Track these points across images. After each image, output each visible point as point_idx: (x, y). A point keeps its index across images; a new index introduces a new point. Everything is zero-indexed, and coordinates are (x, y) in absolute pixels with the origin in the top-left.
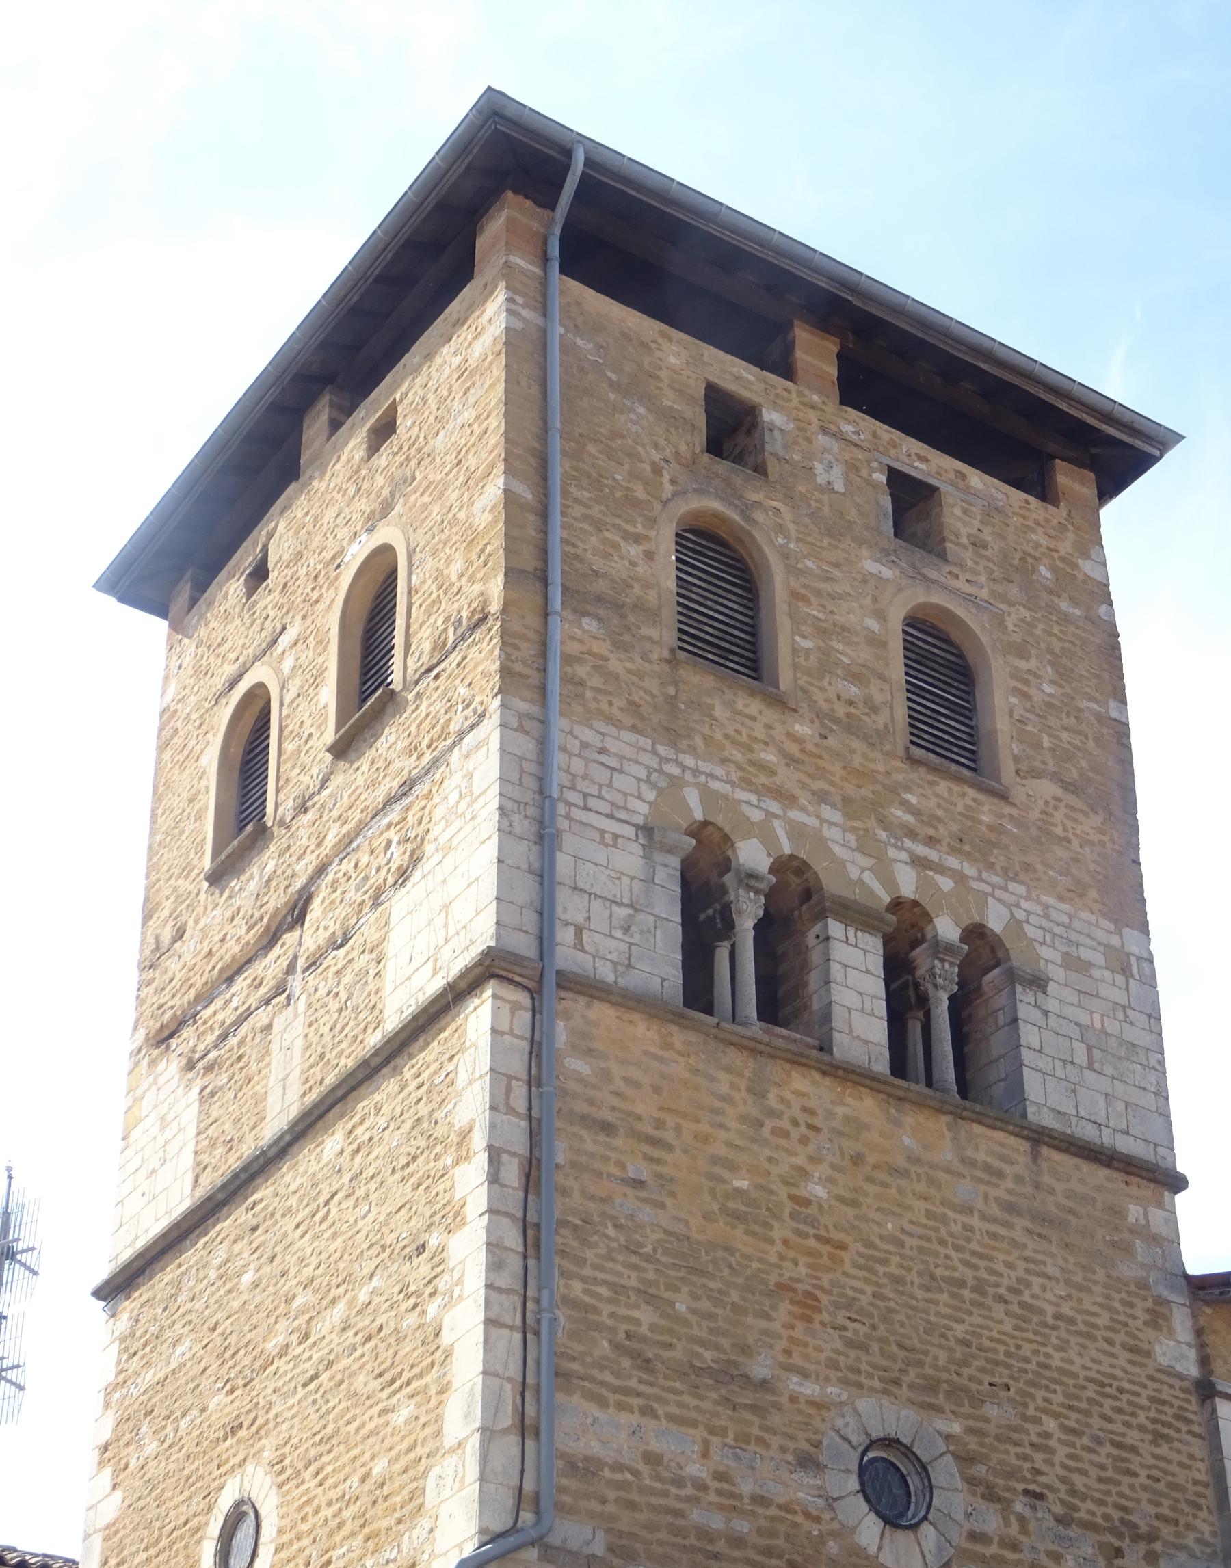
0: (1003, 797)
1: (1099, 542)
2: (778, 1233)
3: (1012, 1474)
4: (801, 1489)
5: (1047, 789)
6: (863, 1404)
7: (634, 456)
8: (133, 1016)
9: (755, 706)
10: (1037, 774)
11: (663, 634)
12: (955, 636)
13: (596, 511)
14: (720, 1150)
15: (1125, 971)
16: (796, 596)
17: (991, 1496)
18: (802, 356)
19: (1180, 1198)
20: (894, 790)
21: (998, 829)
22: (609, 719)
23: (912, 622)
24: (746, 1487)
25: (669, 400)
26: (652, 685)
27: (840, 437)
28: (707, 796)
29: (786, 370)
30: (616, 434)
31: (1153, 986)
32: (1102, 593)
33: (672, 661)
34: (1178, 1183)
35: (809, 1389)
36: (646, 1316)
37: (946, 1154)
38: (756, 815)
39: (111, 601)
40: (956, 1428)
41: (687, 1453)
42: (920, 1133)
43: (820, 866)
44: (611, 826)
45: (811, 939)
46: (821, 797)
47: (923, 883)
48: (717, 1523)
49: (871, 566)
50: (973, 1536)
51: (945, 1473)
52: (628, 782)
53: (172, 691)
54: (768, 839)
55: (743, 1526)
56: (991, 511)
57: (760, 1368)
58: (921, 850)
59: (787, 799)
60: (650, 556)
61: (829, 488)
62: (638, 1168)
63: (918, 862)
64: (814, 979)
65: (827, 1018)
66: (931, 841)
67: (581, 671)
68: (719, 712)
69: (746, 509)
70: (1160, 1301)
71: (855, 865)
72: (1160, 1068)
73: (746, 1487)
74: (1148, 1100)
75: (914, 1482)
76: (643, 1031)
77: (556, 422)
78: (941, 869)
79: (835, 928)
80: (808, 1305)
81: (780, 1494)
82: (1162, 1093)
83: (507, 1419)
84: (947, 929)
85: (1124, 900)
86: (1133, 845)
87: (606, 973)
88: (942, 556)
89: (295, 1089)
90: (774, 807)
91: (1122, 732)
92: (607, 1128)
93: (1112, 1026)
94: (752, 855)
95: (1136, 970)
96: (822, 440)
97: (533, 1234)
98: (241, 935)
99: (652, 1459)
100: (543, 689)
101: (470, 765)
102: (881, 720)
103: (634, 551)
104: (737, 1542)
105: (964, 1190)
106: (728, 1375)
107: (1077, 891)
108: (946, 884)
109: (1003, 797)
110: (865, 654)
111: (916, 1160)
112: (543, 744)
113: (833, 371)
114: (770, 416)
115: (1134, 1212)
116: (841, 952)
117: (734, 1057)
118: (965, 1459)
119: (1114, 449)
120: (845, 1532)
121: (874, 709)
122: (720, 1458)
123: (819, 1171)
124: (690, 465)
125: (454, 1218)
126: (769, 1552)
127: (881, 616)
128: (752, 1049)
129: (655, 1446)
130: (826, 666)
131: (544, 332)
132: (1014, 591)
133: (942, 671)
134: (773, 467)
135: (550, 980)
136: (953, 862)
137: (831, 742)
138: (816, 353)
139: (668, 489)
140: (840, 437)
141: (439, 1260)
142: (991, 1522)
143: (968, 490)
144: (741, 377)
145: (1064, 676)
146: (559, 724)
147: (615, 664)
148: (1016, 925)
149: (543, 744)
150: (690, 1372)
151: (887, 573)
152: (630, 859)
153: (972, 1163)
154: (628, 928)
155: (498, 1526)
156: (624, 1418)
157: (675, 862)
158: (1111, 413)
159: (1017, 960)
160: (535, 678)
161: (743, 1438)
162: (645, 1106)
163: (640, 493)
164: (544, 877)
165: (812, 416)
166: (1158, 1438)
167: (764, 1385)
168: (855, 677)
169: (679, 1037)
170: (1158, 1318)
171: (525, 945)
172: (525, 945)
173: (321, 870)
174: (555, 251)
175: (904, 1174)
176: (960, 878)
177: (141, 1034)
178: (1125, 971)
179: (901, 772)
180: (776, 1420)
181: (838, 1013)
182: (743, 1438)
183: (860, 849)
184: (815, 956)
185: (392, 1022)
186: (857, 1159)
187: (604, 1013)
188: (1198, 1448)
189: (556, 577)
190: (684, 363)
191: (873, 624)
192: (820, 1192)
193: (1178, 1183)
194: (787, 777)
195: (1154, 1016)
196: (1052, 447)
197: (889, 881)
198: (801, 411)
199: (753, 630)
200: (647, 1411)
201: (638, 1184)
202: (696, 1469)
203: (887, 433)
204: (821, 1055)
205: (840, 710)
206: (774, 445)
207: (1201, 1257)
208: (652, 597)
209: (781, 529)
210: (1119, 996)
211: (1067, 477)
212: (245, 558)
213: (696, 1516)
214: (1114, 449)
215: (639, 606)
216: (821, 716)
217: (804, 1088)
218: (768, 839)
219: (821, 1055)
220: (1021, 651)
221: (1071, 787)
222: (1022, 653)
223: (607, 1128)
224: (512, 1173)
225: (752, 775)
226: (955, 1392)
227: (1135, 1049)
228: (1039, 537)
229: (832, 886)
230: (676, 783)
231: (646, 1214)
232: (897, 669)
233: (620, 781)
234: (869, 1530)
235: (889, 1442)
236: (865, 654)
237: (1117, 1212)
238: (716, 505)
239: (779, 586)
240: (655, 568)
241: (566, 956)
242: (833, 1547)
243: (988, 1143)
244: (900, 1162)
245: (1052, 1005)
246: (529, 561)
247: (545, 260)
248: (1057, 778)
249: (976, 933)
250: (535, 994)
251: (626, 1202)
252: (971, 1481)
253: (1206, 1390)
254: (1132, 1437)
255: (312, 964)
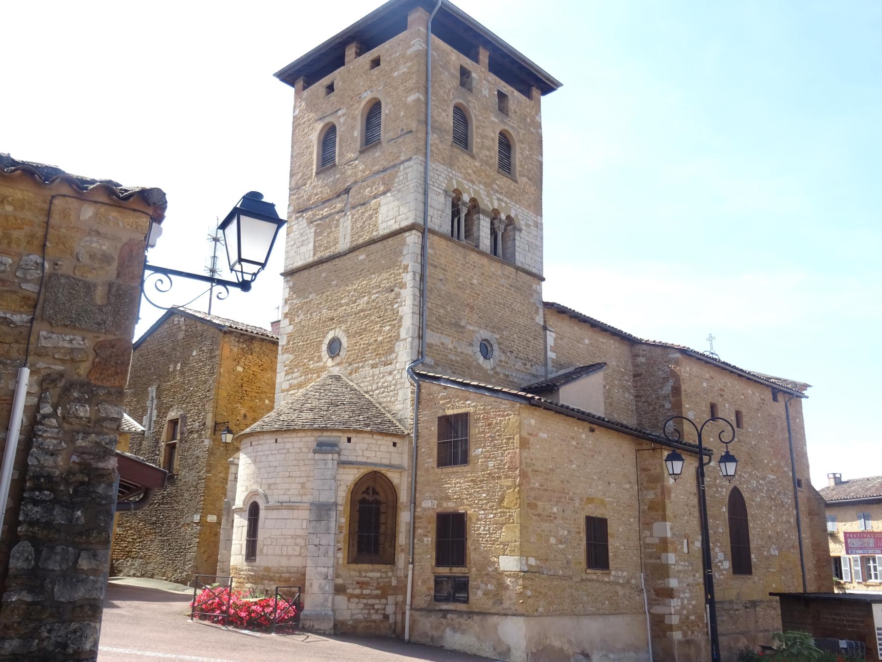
0: (516, 182)
1: (540, 111)
2: (468, 291)
3: (507, 347)
4: (469, 351)
5: (525, 179)
7: (444, 87)
9: (468, 158)
12: (508, 137)
14: (457, 272)
15: (537, 227)
16: (477, 127)
17: (504, 352)
19: (543, 283)
20: (494, 180)
21: (514, 190)
22: (438, 162)
23: (501, 133)
24: (459, 350)
25: (452, 70)
26: (447, 152)
27: (488, 81)
28: (458, 182)
29: (476, 60)
30: (441, 81)
31: (542, 230)
32: (539, 126)
33: (452, 146)
34: (543, 279)
35: (472, 328)
36: (442, 311)
37: (499, 273)
40: (498, 337)
41: (449, 342)
42: (494, 268)
43: (479, 200)
44: (438, 190)
46: (480, 182)
47: (499, 205)
48: (454, 358)
49: (493, 119)
50: (500, 361)
51: (496, 347)
53: (297, 112)
54: (469, 194)
55: (458, 359)
56: (519, 102)
57: (463, 324)
58: (499, 196)
59: (473, 182)
60: (447, 115)
61: (485, 96)
62: (441, 276)
63: (499, 199)
64: (475, 228)
65: (478, 238)
66: (501, 194)
67: (433, 148)
68: (461, 160)
70: (538, 308)
71: (488, 202)
72: (542, 252)
73: (459, 350)
74: (539, 259)
75: (489, 348)
76: (443, 243)
77: (430, 79)
78: (502, 201)
79: (481, 216)
81: (465, 351)
83: (416, 335)
84: (503, 216)
87: (437, 228)
89: (348, 239)
90: (470, 185)
92: (436, 267)
93: (533, 241)
94: (466, 198)
95: (539, 226)
96: (484, 82)
98: (327, 192)
99: (442, 344)
100: (426, 154)
101: (407, 171)
102: (493, 161)
103: (444, 114)
104: (457, 362)
105: (503, 281)
106: (457, 325)
107: (529, 207)
108: (503, 205)
109: (516, 182)
111: (494, 274)
112: (426, 168)
113: (487, 61)
114: (474, 75)
115: (534, 286)
117: (460, 249)
118: (499, 344)
119: (547, 85)
121: (491, 158)
123: (476, 277)
124: (456, 89)
125: (403, 286)
126: (463, 364)
127: (494, 132)
128: (464, 247)
129: (443, 341)
130: (482, 147)
131: (427, 51)
132: (522, 126)
133: (505, 144)
135: (426, 230)
136: (505, 199)
137: (483, 167)
138: (484, 56)
139: (452, 96)
140: (488, 81)
141: (398, 295)
142: (503, 358)
144: (468, 63)
145: (531, 149)
146: (429, 163)
147: (440, 147)
148: (517, 215)
149: (426, 168)
150: (450, 324)
151: (496, 120)
152: (441, 199)
153: (504, 275)
154: (440, 219)
155: (415, 358)
156: (438, 335)
157: (451, 199)
158: (549, 78)
160: (424, 151)
161: (459, 339)
162: (443, 261)
163: (446, 98)
164: (425, 204)
165: (482, 75)
166: (535, 339)
168: (489, 150)
169: (450, 244)
172: (421, 222)
173: (355, 182)
175: (491, 277)
176: (506, 203)
177: (292, 208)
178: (537, 227)
179: (497, 176)
180: (465, 335)
181: (481, 238)
182: (459, 339)
183: (487, 196)
184: (476, 223)
185: (382, 232)
186: (483, 274)
187: (436, 238)
188: (542, 341)
189: (429, 124)
190: (456, 58)
191: (492, 135)
193: (543, 279)
194: (473, 177)
195: (542, 239)
196: (532, 83)
197: (492, 204)
199: (466, 135)
200: (442, 333)
201: (441, 280)
202: (450, 346)
203: (498, 80)
204: (476, 248)
205: (485, 158)
206: (474, 84)
207: (546, 298)
209: (475, 108)
210: (535, 233)
211: (535, 92)
213: (450, 356)
214: (547, 85)
215: (445, 130)
216: (481, 160)
217: (474, 256)
218: (469, 194)
222: (523, 143)
223: (436, 267)
224: (418, 278)
225: (467, 177)
226: (498, 328)
227: (537, 247)
228: (528, 110)
229: (481, 206)
230: (451, 179)
231: (443, 287)
232: (497, 148)
237: (531, 286)
238: (461, 101)
240: (447, 119)
241: (430, 225)
242: (474, 363)
243: (509, 270)
244: (491, 274)
245: (522, 236)
247: (427, 29)
249: (508, 217)
250: (423, 233)
251: (439, 284)
252: (500, 349)
253: (545, 328)
254: (530, 339)
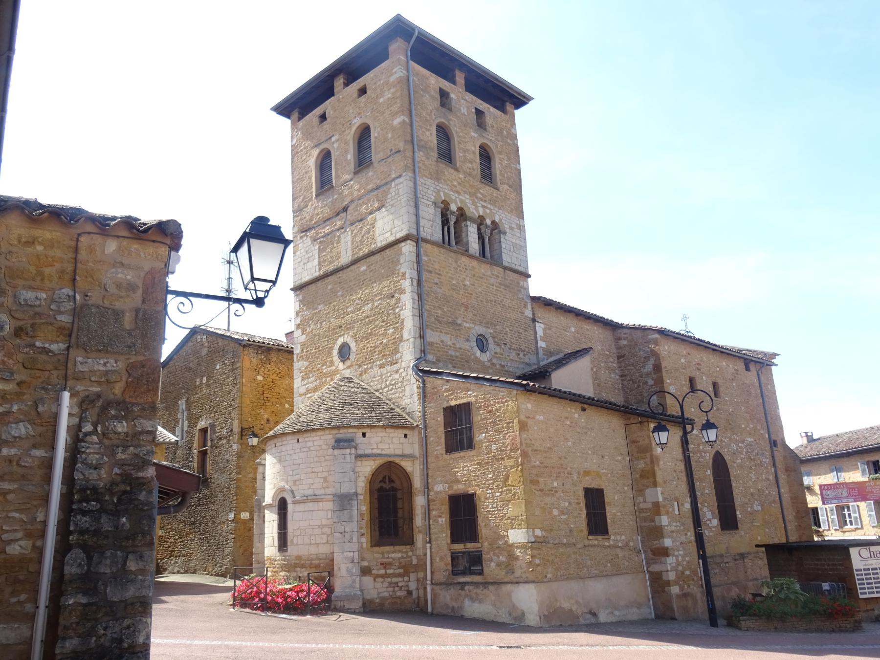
3: (501, 340)
4: (466, 346)
5: (506, 187)
6: (477, 327)
8: (292, 224)
9: (452, 171)
10: (504, 183)
11: (435, 154)
13: (421, 123)
14: (450, 275)
16: (459, 143)
17: (498, 345)
18: (457, 79)
19: (529, 279)
24: (458, 346)
25: (433, 93)
26: (433, 167)
27: (465, 100)
28: (445, 194)
31: (524, 231)
33: (437, 161)
34: (529, 276)
35: (467, 325)
36: (439, 312)
37: (489, 273)
38: (454, 198)
39: (274, 113)
41: (448, 340)
42: (484, 269)
45: (463, 224)
47: (484, 211)
49: (473, 134)
51: (490, 340)
52: (430, 190)
54: (456, 204)
55: (458, 354)
56: (495, 117)
57: (459, 322)
59: (459, 193)
60: (431, 134)
62: (436, 280)
63: (483, 207)
65: (467, 244)
66: (485, 201)
67: (420, 165)
69: (449, 120)
71: (474, 209)
72: (526, 251)
75: (485, 342)
76: (436, 250)
78: (487, 208)
79: (469, 223)
80: (466, 307)
81: (463, 347)
82: (526, 257)
83: (418, 335)
84: (488, 222)
85: (518, 210)
86: (521, 199)
87: (429, 237)
88: (485, 129)
91: (519, 172)
92: (431, 272)
94: (453, 207)
95: (521, 228)
97: (420, 296)
99: (442, 341)
103: (428, 133)
104: (457, 357)
106: (454, 323)
107: (511, 211)
108: (488, 211)
110: (472, 156)
112: (415, 183)
114: (452, 96)
115: (521, 283)
116: (470, 229)
117: (452, 254)
118: (494, 337)
119: (519, 100)
120: (474, 354)
122: (454, 341)
123: (468, 279)
125: (402, 291)
127: (474, 146)
128: (455, 252)
129: (443, 338)
134: (453, 109)
136: (489, 206)
138: (460, 77)
140: (465, 100)
141: (399, 300)
142: (498, 350)
143: (490, 112)
144: (446, 85)
145: (509, 159)
146: (418, 178)
147: (427, 163)
149: (415, 183)
150: (448, 323)
152: (431, 210)
155: (418, 357)
158: (521, 93)
159: (501, 228)
166: (526, 331)
167: (460, 325)
168: (471, 162)
169: (442, 250)
170: (525, 306)
171: (414, 232)
172: (414, 232)
173: (352, 201)
174: (409, 54)
176: (490, 210)
177: (296, 229)
180: (462, 332)
184: (464, 229)
186: (474, 275)
187: (429, 246)
188: (532, 332)
189: (415, 143)
191: (473, 148)
192: (468, 283)
193: (529, 276)
194: (459, 188)
195: (525, 239)
197: (478, 212)
198: (459, 95)
199: (450, 151)
201: (437, 284)
202: (449, 343)
204: (466, 252)
205: (468, 171)
206: (453, 104)
208: (432, 145)
211: (509, 107)
212: (318, 111)
213: (450, 352)
214: (519, 100)
216: (465, 173)
217: (464, 260)
218: (456, 204)
219: (466, 252)
220: (501, 153)
221: (510, 186)
223: (431, 272)
224: (415, 283)
227: (521, 248)
229: (468, 214)
230: (439, 191)
231: (438, 290)
232: (478, 160)
233: (429, 192)
234: (478, 353)
235: (481, 335)
236: (472, 156)
238: (443, 120)
239: (456, 139)
240: (431, 137)
241: (423, 234)
243: (498, 270)
246: (409, 138)
247: (407, 57)
248: (508, 184)
249: (493, 222)
250: (417, 243)
251: (435, 288)
253: (534, 320)
254: (521, 331)
255: (352, 224)
